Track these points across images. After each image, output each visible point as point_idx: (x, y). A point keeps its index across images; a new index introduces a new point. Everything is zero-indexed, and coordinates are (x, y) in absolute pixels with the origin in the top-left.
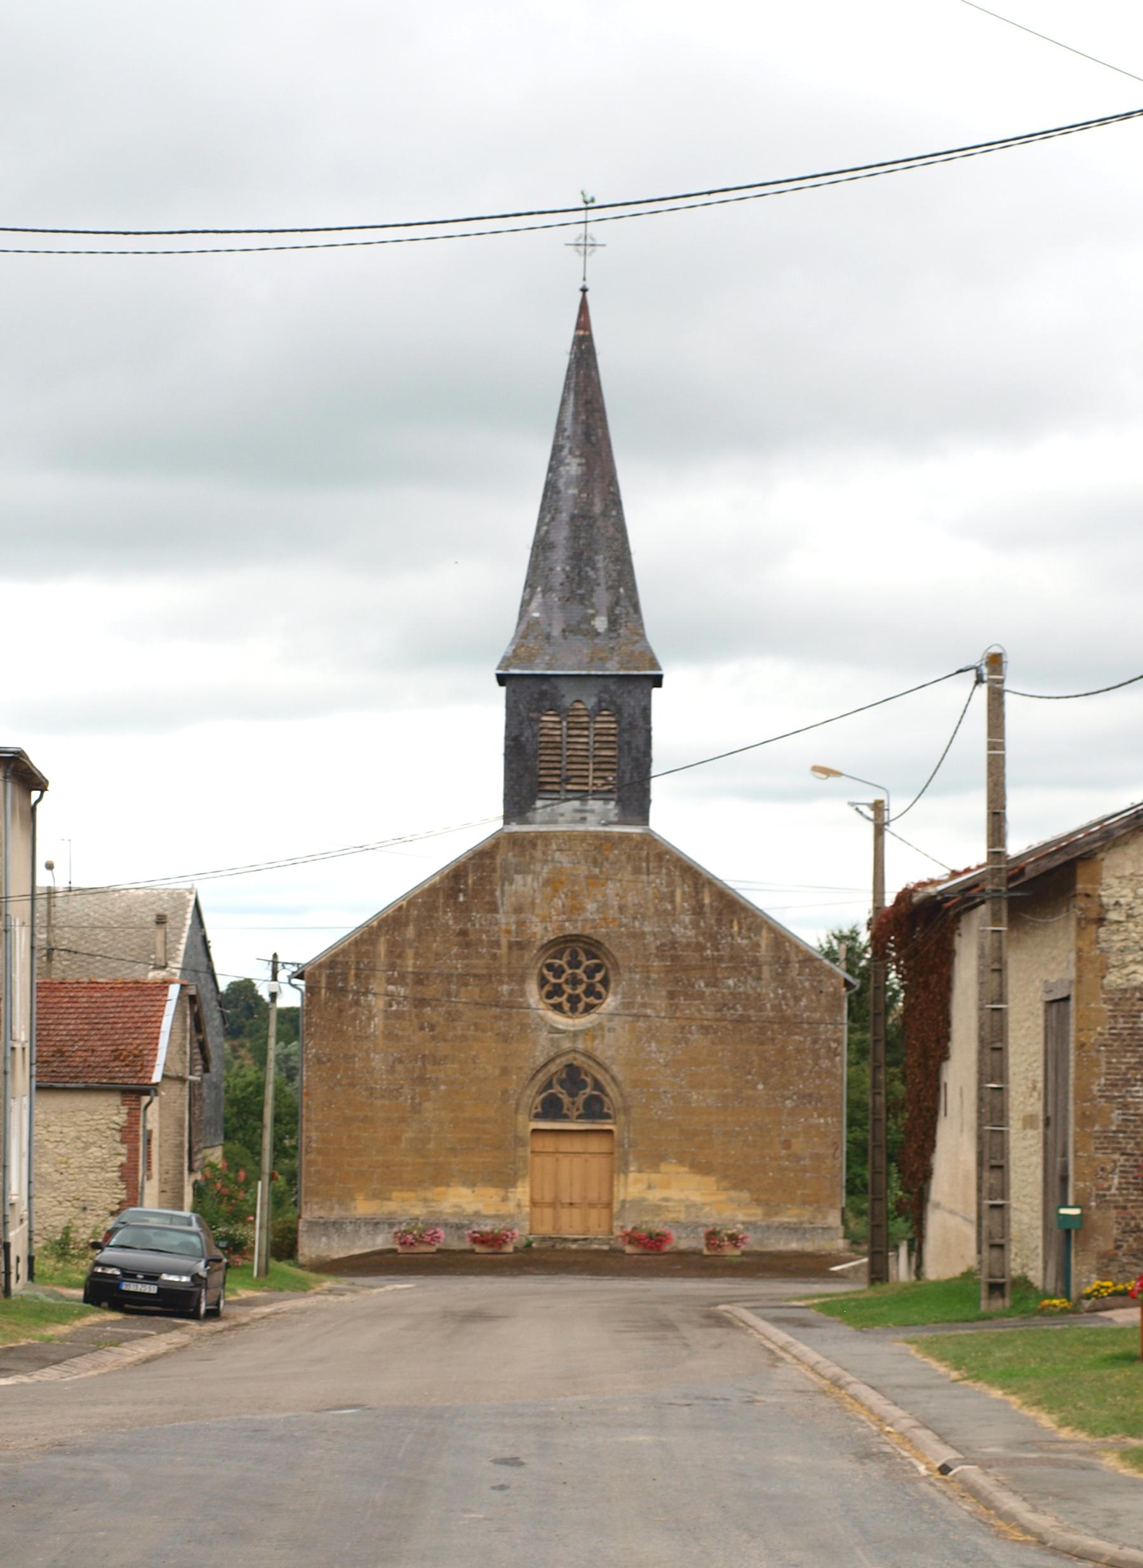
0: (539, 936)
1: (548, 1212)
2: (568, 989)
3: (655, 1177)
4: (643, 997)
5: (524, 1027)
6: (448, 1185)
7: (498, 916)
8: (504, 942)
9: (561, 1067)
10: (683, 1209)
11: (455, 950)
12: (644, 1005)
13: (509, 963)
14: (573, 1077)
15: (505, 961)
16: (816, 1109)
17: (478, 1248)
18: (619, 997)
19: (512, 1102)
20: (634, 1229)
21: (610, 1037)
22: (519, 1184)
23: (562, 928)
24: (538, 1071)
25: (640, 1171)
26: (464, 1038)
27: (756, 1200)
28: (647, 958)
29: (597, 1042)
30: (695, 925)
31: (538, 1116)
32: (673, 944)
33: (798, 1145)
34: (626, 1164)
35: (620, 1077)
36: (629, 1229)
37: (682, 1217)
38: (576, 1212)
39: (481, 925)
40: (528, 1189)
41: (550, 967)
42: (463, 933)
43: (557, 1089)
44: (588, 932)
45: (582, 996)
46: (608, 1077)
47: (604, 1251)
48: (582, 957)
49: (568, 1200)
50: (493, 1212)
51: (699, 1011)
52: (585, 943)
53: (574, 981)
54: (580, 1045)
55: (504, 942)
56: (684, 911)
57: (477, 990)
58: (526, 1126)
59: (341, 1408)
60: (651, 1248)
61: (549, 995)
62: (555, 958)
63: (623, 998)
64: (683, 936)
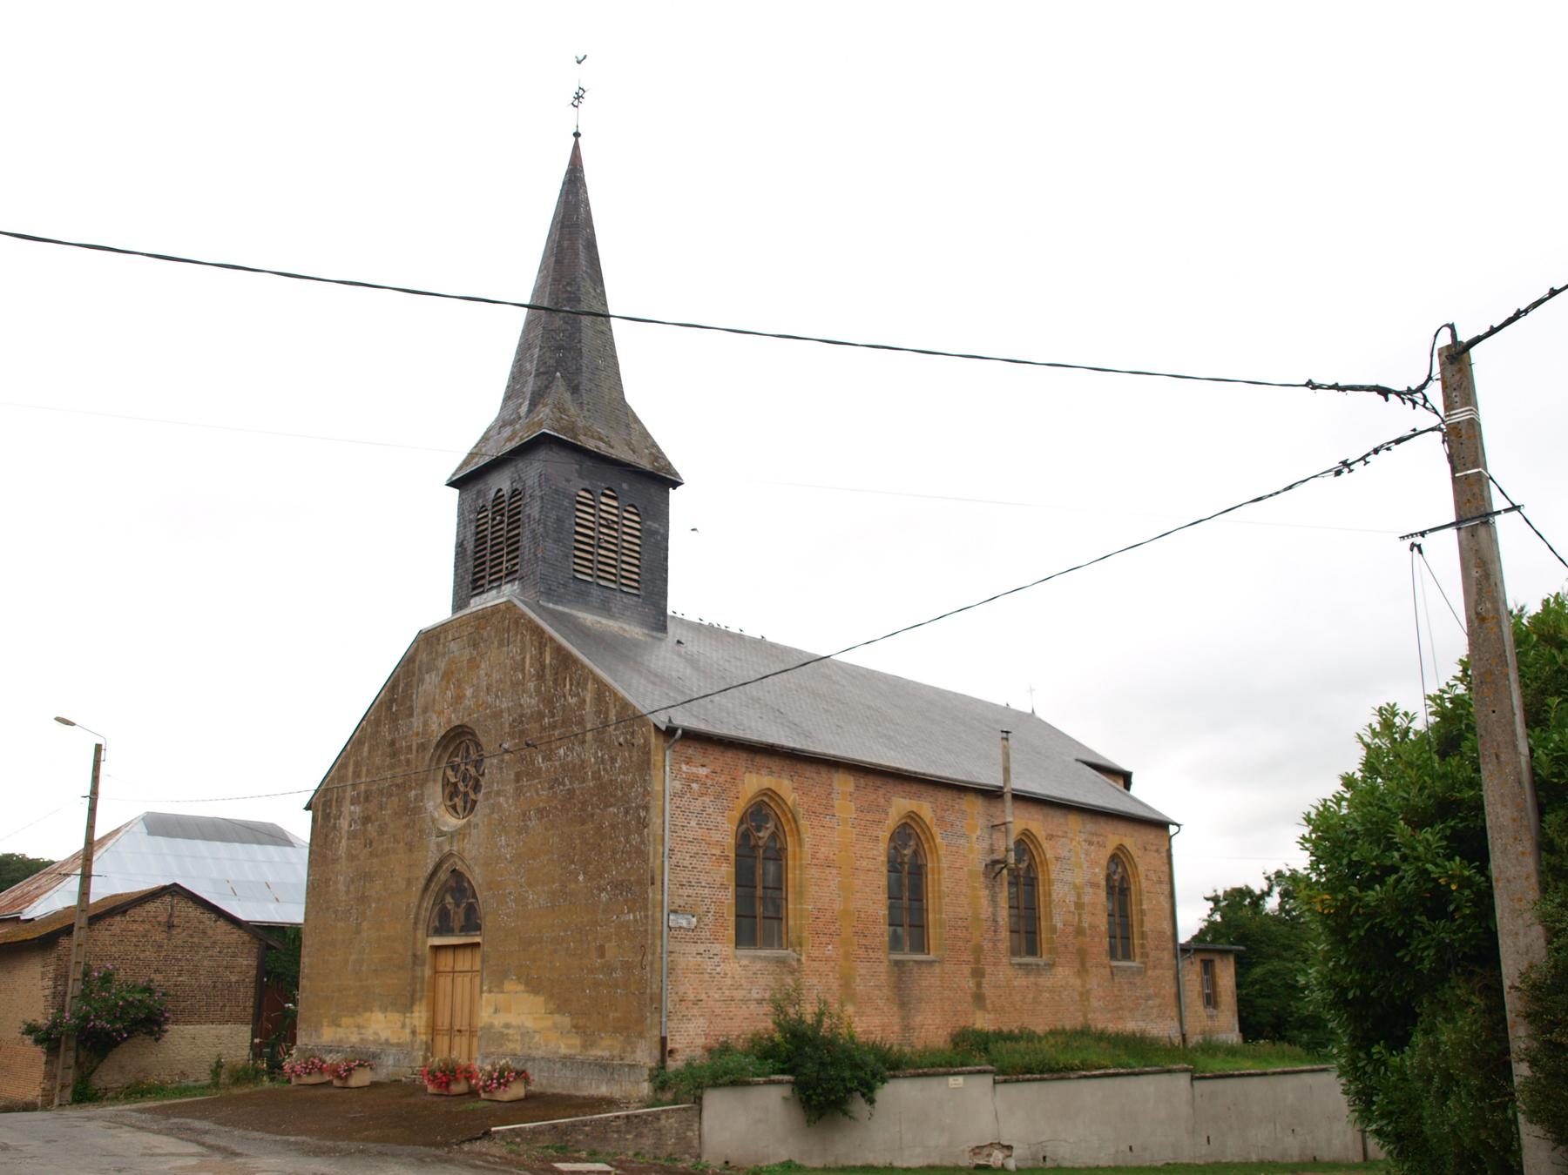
16: (626, 901)
22: (416, 1008)
23: (449, 721)
25: (490, 991)
27: (576, 1026)
31: (438, 932)
33: (611, 948)
40: (424, 1015)
58: (424, 943)
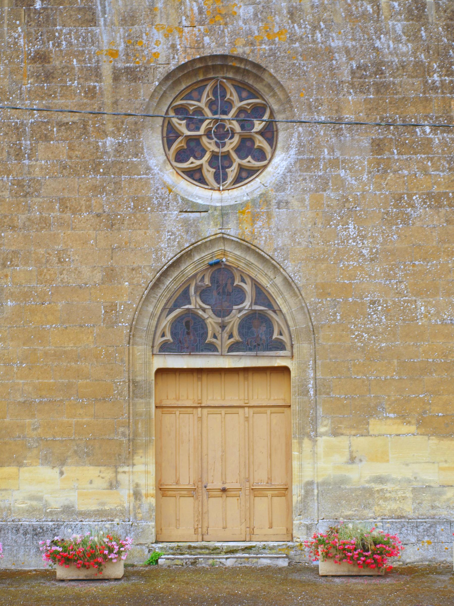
0: (162, 59)
1: (187, 506)
2: (210, 145)
3: (360, 442)
4: (332, 150)
5: (139, 203)
6: (20, 465)
7: (97, 30)
8: (107, 70)
9: (202, 267)
10: (409, 495)
11: (28, 84)
12: (334, 164)
13: (116, 103)
14: (221, 282)
15: (108, 100)
17: (61, 572)
18: (293, 152)
19: (124, 325)
20: (333, 531)
21: (280, 216)
24: (165, 274)
25: (335, 433)
26: (45, 223)
28: (336, 88)
29: (259, 224)
30: (413, 36)
31: (166, 349)
32: (378, 67)
34: (314, 422)
35: (299, 281)
36: (322, 530)
37: (408, 509)
38: (232, 503)
39: (70, 44)
40: (152, 468)
41: (180, 111)
42: (42, 58)
43: (195, 303)
44: (239, 51)
45: (234, 155)
46: (279, 281)
47: (281, 570)
48: (232, 95)
49: (220, 486)
50: (94, 507)
51: (425, 170)
52: (237, 70)
53: (222, 134)
54: (232, 230)
55: (107, 70)
56: (393, 15)
57: (64, 146)
58: (148, 364)
59: (246, 370)
60: (366, 564)
61: (181, 157)
62: (189, 97)
63: (299, 153)
64: (395, 53)
